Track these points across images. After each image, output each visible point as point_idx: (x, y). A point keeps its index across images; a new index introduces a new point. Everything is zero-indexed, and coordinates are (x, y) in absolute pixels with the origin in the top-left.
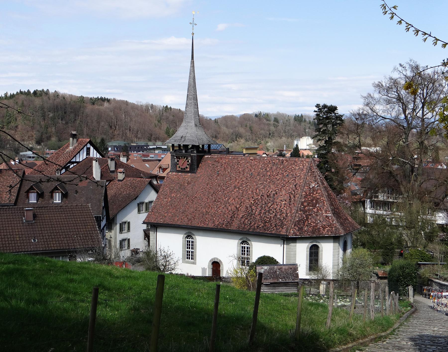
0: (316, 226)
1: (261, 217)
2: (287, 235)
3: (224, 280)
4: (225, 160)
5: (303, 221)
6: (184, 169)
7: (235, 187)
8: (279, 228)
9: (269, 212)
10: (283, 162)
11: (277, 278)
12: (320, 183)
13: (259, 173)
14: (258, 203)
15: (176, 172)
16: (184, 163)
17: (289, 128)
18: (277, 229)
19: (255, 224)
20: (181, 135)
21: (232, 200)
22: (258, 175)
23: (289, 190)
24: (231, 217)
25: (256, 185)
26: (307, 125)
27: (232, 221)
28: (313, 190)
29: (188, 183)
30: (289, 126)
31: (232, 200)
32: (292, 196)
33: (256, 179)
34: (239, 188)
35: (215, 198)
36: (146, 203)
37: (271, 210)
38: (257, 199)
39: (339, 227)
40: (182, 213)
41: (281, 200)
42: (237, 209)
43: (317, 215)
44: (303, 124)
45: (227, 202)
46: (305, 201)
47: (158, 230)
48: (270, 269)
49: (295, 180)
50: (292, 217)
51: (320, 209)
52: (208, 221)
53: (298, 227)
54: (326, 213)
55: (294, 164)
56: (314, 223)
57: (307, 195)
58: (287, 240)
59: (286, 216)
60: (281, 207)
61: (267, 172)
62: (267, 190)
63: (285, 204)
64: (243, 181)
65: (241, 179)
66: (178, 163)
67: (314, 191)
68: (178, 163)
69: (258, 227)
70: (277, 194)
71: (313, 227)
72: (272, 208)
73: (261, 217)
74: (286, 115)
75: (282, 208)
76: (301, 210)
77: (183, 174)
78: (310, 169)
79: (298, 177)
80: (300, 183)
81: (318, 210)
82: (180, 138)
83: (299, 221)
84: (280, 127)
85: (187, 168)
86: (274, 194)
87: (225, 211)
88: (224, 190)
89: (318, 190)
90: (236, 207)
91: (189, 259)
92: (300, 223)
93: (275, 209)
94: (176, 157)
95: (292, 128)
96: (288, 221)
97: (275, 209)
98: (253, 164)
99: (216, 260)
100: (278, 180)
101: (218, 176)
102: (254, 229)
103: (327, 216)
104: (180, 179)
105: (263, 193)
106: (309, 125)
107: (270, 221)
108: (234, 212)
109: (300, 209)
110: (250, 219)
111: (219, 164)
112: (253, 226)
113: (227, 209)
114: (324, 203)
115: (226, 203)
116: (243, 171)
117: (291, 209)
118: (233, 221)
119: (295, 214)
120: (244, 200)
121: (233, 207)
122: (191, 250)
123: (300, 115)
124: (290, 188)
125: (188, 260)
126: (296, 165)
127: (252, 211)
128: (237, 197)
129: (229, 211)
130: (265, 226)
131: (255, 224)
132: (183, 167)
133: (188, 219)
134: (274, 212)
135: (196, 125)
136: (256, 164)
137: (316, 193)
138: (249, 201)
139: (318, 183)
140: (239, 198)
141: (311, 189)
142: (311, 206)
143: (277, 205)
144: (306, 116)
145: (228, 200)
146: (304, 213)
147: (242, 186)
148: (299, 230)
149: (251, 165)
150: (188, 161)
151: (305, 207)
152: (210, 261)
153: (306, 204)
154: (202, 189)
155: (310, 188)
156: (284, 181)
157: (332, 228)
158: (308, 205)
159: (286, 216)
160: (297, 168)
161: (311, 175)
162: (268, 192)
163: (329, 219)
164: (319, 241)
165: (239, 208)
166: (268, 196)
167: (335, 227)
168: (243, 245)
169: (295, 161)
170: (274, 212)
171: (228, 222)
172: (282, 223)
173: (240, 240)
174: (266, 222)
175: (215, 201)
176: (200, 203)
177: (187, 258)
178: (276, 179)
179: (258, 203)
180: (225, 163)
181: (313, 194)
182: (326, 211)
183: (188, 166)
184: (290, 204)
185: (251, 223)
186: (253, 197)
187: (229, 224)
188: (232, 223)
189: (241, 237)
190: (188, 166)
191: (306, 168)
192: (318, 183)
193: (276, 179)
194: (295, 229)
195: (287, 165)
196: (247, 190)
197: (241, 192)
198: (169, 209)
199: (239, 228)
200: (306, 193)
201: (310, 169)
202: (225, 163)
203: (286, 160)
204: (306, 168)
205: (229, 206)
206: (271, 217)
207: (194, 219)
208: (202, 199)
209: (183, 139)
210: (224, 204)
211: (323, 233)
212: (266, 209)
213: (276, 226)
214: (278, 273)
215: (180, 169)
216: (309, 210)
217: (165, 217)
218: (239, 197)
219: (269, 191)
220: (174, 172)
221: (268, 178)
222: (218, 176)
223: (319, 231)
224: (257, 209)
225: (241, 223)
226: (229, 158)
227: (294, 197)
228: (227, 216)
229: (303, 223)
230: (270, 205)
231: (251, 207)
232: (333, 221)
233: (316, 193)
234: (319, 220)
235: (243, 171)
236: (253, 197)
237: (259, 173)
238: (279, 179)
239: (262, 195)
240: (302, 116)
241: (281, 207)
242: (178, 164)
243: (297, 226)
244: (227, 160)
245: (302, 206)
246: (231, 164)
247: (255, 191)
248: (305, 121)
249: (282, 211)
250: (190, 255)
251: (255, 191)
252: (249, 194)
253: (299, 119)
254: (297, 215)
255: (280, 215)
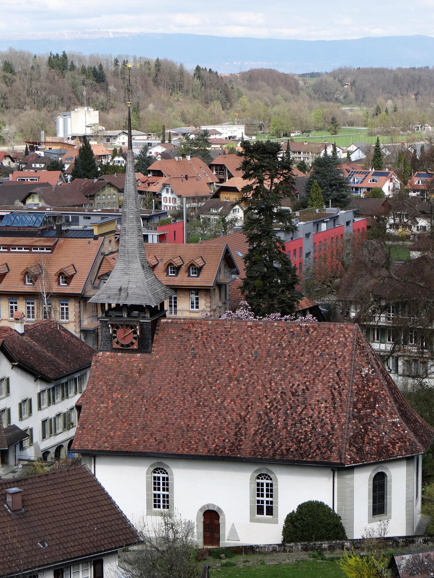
0: (381, 442)
1: (289, 432)
2: (341, 464)
3: (258, 550)
4: (201, 328)
5: (360, 435)
6: (128, 346)
7: (230, 379)
8: (326, 451)
9: (301, 423)
10: (308, 331)
11: (427, 572)
12: (375, 366)
13: (269, 351)
14: (279, 407)
15: (111, 351)
16: (125, 336)
17: (39, 84)
18: (322, 453)
19: (281, 445)
20: (119, 285)
21: (230, 403)
22: (268, 355)
23: (329, 382)
24: (236, 434)
25: (269, 374)
26: (77, 77)
27: (239, 441)
28: (367, 380)
29: (139, 373)
30: (38, 80)
31: (230, 403)
32: (336, 394)
33: (265, 362)
34: (238, 381)
35: (197, 399)
36: (64, 414)
37: (305, 419)
38: (275, 399)
39: (415, 440)
40: (143, 429)
41: (318, 401)
42: (243, 418)
43: (379, 423)
44: (68, 74)
45: (220, 407)
46: (358, 401)
47: (97, 460)
48: (414, 558)
49: (335, 363)
50: (342, 430)
51: (382, 411)
52: (196, 443)
53: (356, 448)
54: (392, 417)
55: (328, 334)
56: (377, 437)
57: (359, 390)
58: (339, 469)
59: (333, 428)
60: (319, 413)
61: (283, 349)
62: (290, 382)
63: (326, 407)
64: (243, 367)
65: (239, 363)
66: (114, 335)
67: (368, 381)
68: (114, 335)
69: (288, 450)
70: (308, 390)
71: (378, 444)
72: (305, 414)
73: (289, 432)
74: (30, 55)
75: (323, 415)
76: (354, 417)
77: (127, 355)
78: (358, 343)
79: (340, 357)
80: (346, 369)
81: (379, 414)
82: (117, 292)
83: (355, 437)
84: (17, 84)
85: (132, 343)
86: (303, 390)
87: (221, 423)
88: (212, 384)
89: (374, 379)
90: (240, 416)
91: (159, 507)
92: (357, 440)
93: (311, 417)
94: (112, 325)
95: (44, 84)
96: (337, 438)
97: (311, 417)
98: (254, 335)
99: (211, 508)
100: (305, 364)
101: (194, 357)
102: (282, 454)
103: (393, 423)
104: (121, 364)
105: (283, 389)
106: (83, 77)
107: (306, 440)
108: (237, 424)
109: (353, 415)
110: (271, 437)
111: (192, 336)
112: (278, 449)
113: (225, 419)
114: (386, 400)
115: (220, 409)
116: (239, 347)
117: (338, 416)
118: (241, 440)
119: (346, 425)
120: (251, 402)
121: (234, 416)
122: (161, 492)
123: (61, 54)
124: (330, 378)
125: (157, 509)
126: (333, 337)
127: (271, 423)
128: (237, 396)
129: (229, 423)
130: (301, 448)
131: (281, 445)
132: (126, 342)
133: (156, 440)
134: (309, 423)
135: (143, 266)
136: (259, 335)
137: (373, 385)
138: (262, 403)
139: (372, 367)
140: (241, 399)
141: (363, 378)
142: (368, 408)
143: (313, 410)
144: (73, 56)
145: (222, 402)
146: (360, 422)
147: (243, 377)
148: (357, 453)
149: (251, 336)
150: (135, 332)
151: (359, 410)
152: (201, 510)
153: (360, 406)
154: (169, 384)
155: (362, 376)
156: (317, 365)
157: (405, 442)
158: (364, 406)
159: (333, 428)
160: (336, 342)
161: (360, 353)
162: (292, 387)
163: (397, 427)
164: (386, 465)
165: (246, 416)
166: (293, 394)
167: (409, 440)
168: (260, 481)
169: (329, 329)
170: (309, 423)
171: (233, 443)
172: (329, 442)
173: (255, 472)
174: (300, 442)
175: (198, 405)
176: (172, 410)
177: (155, 506)
178: (302, 362)
179: (279, 407)
180: (202, 333)
181: (368, 386)
182: (391, 414)
183: (134, 341)
184: (334, 408)
185: (273, 445)
186: (266, 397)
187: (236, 446)
188: (241, 445)
189: (256, 468)
190: (134, 341)
191: (352, 342)
192: (372, 367)
193: (302, 362)
194: (352, 451)
195: (317, 336)
196: (253, 383)
197: (243, 387)
198: (114, 422)
199: (255, 454)
200: (358, 387)
201: (358, 343)
202: (202, 333)
203: (313, 327)
204: (352, 342)
205: (227, 413)
206: (305, 431)
207: (168, 441)
208: (174, 402)
209: (123, 294)
210: (216, 410)
211: (393, 453)
212: (294, 418)
213: (319, 448)
214: (426, 563)
215: (119, 346)
216: (366, 415)
217: (112, 438)
218: (242, 396)
219: (293, 385)
220: (107, 351)
221: (287, 361)
222: (194, 357)
223: (388, 451)
224: (278, 417)
225: (256, 445)
226: (208, 324)
227: (340, 393)
228: (228, 433)
229: (362, 438)
230: (299, 409)
231: (267, 414)
232: (404, 431)
233: (373, 385)
234: (383, 431)
235: (239, 347)
236: (266, 397)
237: (269, 351)
238: (307, 362)
239: (282, 393)
240: (65, 56)
241: (319, 413)
242: (115, 337)
243: (354, 446)
244: (205, 328)
245: (356, 410)
246: (214, 335)
247: (268, 386)
248: (73, 67)
249: (323, 420)
250: (161, 499)
251: (268, 386)
252: (258, 390)
253: (60, 62)
254: (350, 426)
255: (322, 427)
